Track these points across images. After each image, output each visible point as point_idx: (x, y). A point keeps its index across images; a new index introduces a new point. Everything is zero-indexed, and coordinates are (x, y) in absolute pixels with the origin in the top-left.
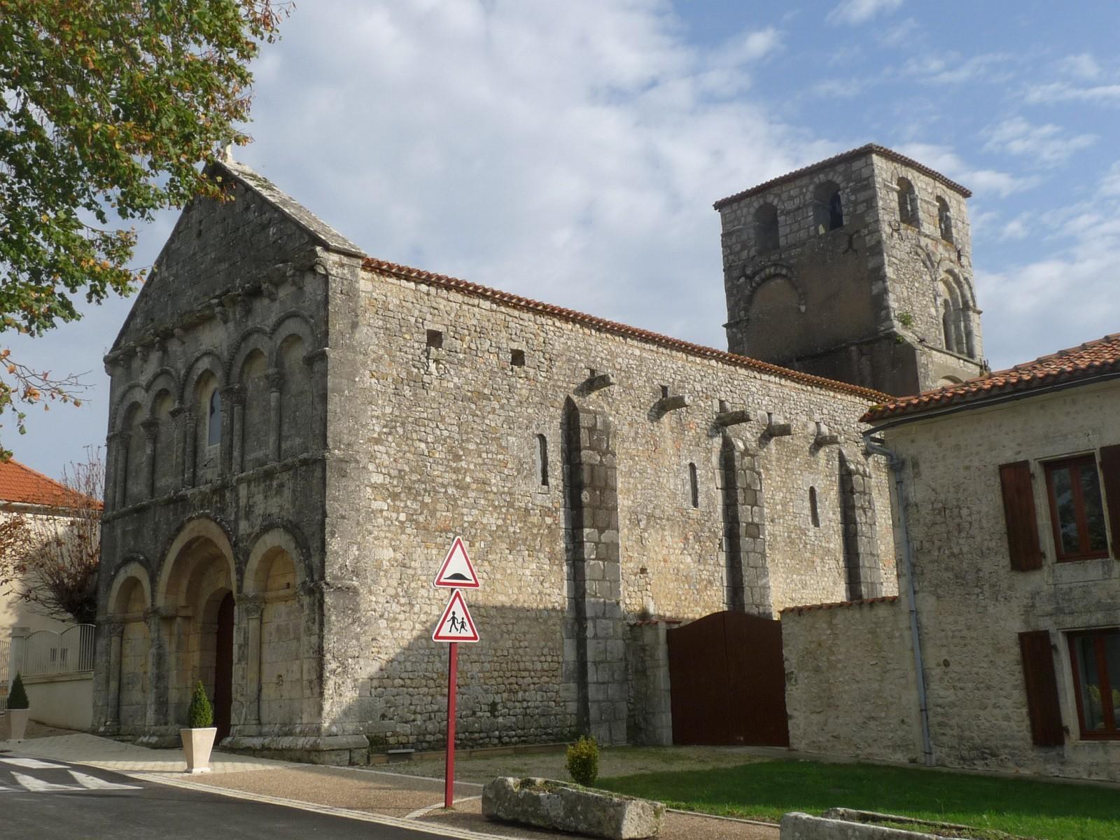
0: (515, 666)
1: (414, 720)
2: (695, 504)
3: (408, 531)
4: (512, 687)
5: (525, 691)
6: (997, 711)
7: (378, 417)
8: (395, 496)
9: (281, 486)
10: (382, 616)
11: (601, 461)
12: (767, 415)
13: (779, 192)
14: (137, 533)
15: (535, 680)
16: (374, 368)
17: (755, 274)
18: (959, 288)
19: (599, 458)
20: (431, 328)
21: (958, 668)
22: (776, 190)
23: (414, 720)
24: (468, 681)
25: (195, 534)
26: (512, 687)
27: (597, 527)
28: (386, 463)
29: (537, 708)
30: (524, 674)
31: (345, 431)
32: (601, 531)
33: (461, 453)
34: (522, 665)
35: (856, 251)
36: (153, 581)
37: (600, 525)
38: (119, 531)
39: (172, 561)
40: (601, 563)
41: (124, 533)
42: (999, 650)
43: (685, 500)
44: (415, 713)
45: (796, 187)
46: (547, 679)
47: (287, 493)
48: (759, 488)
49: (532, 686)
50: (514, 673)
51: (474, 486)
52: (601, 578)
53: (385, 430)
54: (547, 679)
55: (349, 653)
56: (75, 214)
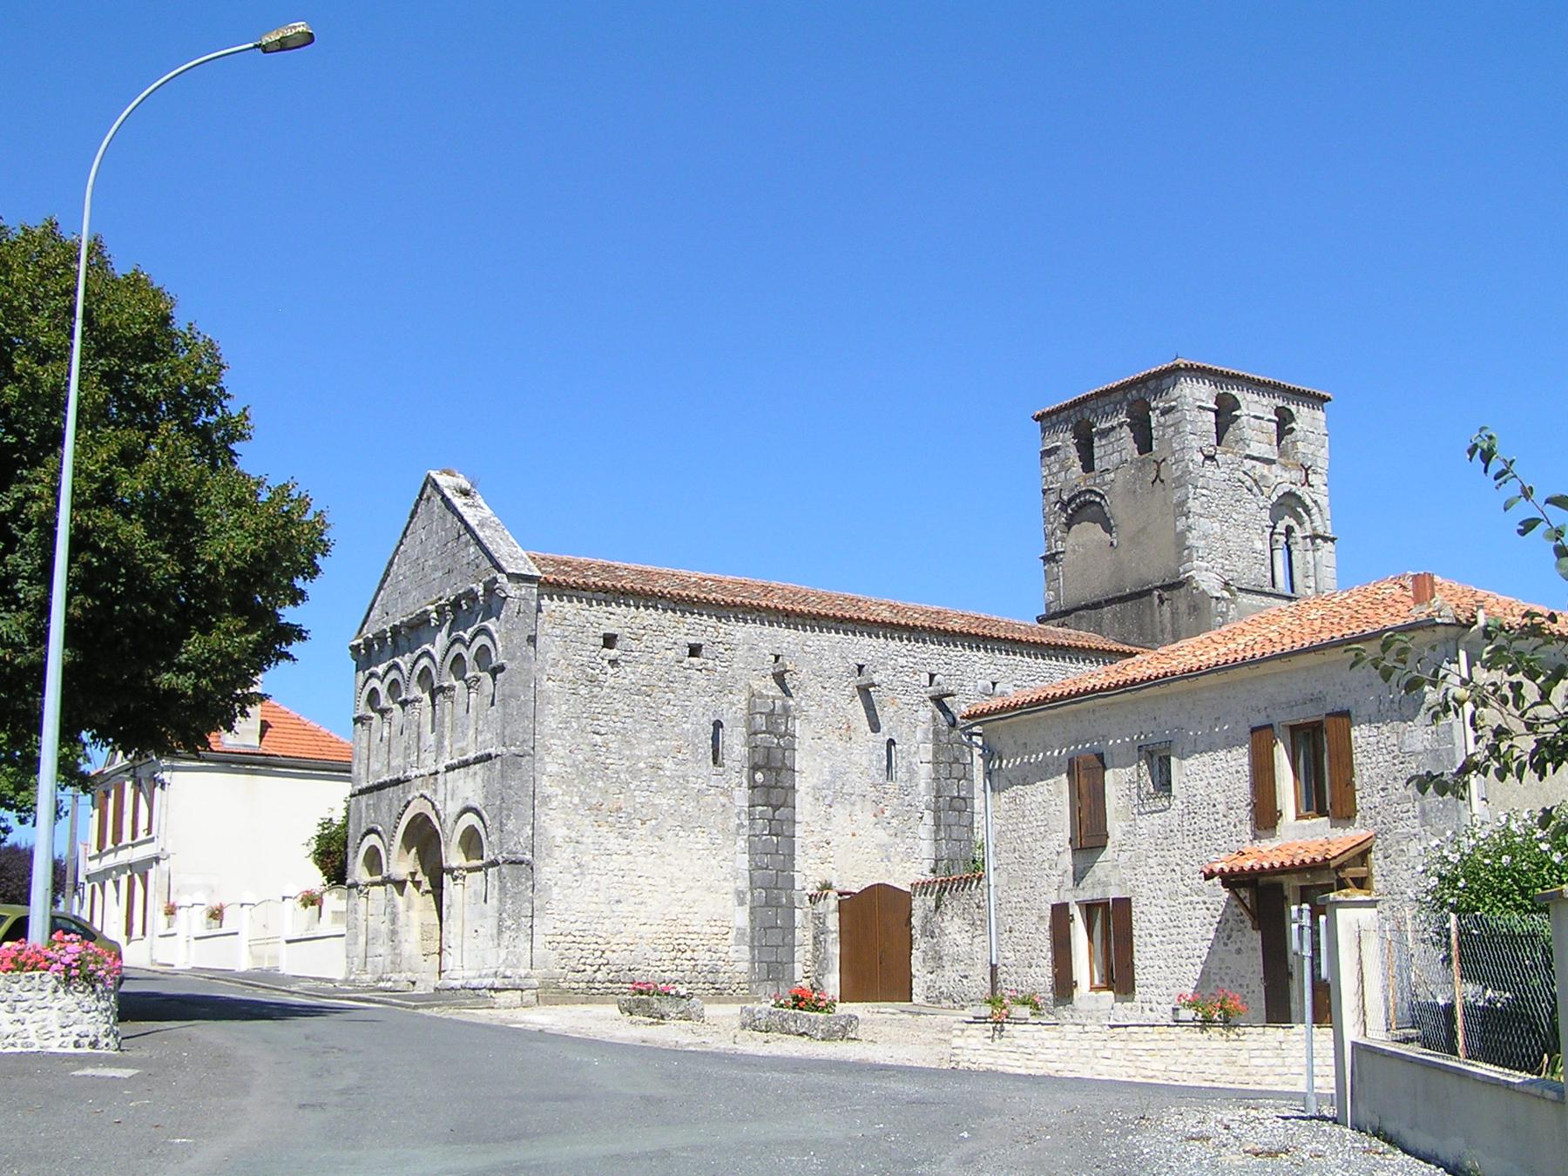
0: (684, 929)
1: (584, 971)
2: (889, 777)
3: (581, 812)
4: (680, 947)
5: (693, 951)
6: (1037, 969)
7: (554, 715)
8: (570, 783)
9: (475, 773)
10: (556, 884)
11: (779, 743)
12: (991, 686)
13: (1095, 407)
14: (376, 807)
15: (705, 942)
16: (552, 672)
17: (1071, 500)
18: (1305, 512)
19: (776, 741)
20: (607, 632)
21: (1017, 934)
22: (1091, 404)
23: (584, 971)
24: (637, 940)
25: (418, 811)
26: (680, 947)
27: (771, 805)
28: (562, 754)
29: (706, 966)
30: (692, 936)
31: (521, 730)
32: (776, 808)
33: (635, 742)
34: (690, 929)
35: (1162, 481)
36: (388, 851)
37: (774, 802)
38: (364, 805)
39: (401, 837)
40: (775, 838)
41: (367, 805)
42: (1041, 918)
43: (881, 776)
44: (584, 964)
45: (1111, 403)
46: (717, 942)
47: (479, 779)
48: (969, 761)
49: (701, 947)
50: (682, 935)
51: (647, 771)
52: (774, 851)
53: (560, 726)
54: (717, 942)
55: (523, 913)
56: (269, 666)
